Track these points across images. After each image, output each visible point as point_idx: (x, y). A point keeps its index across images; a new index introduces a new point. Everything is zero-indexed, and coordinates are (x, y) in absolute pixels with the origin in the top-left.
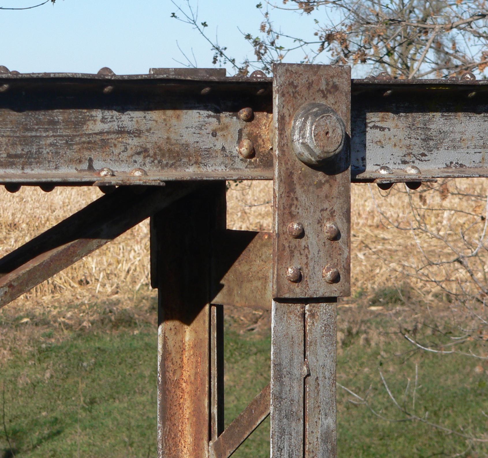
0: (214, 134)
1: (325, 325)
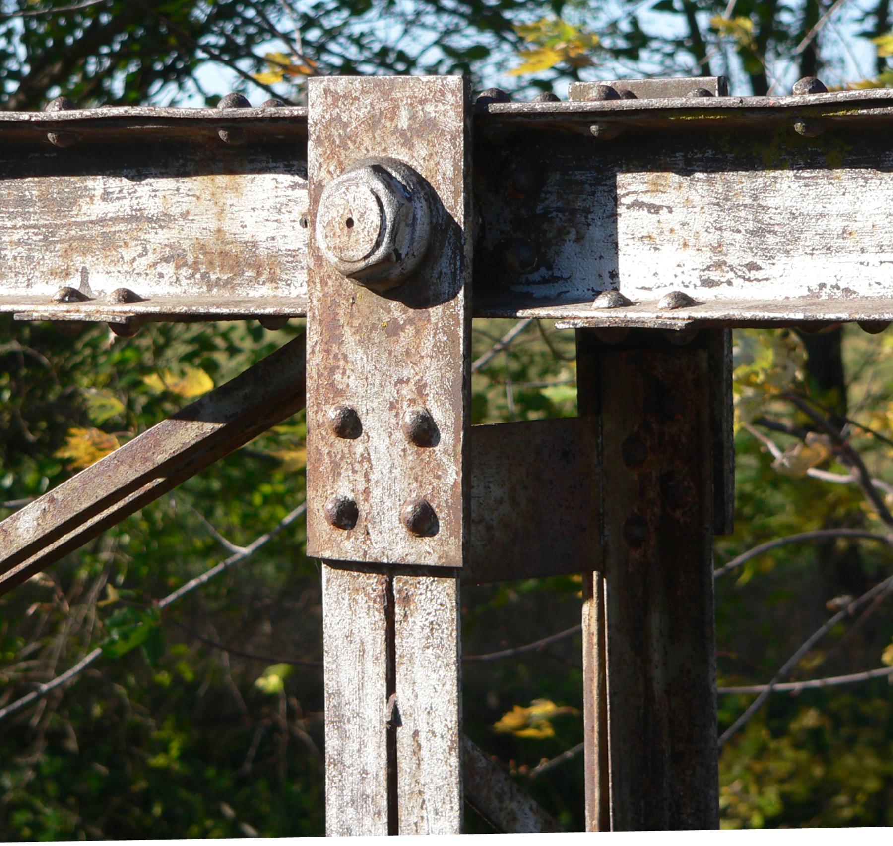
1: (432, 623)
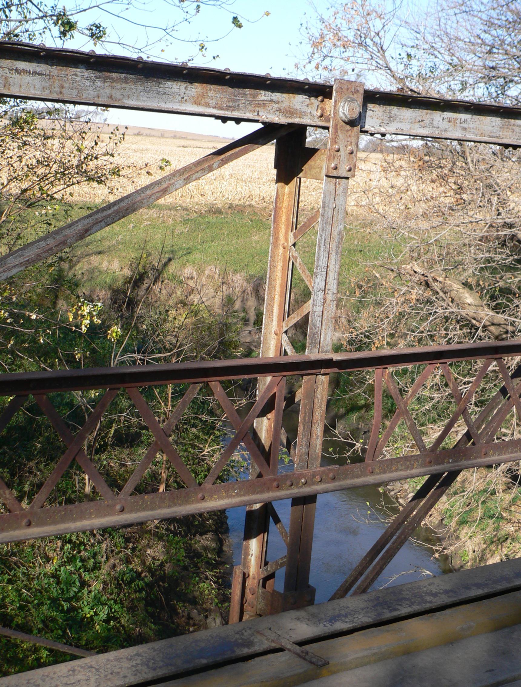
0: (308, 106)
